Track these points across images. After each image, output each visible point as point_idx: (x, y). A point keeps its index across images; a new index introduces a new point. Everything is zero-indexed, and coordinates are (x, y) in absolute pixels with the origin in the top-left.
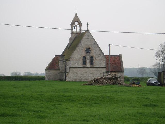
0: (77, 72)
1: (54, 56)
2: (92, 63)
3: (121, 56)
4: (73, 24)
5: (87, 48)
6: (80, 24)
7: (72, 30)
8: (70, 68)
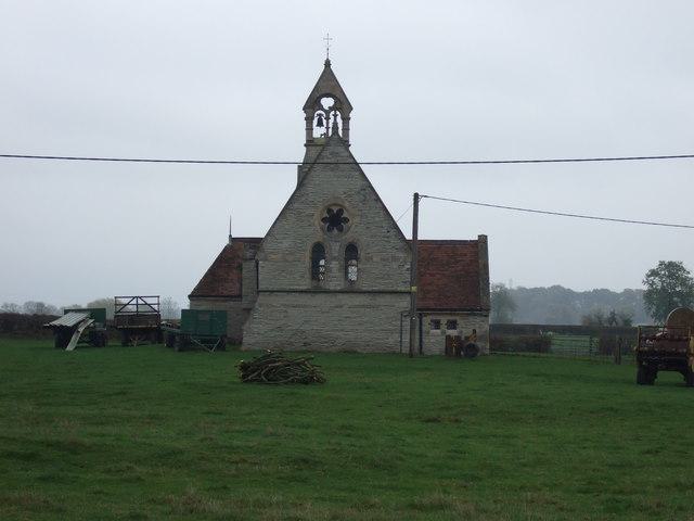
0: (286, 311)
1: (226, 242)
4: (312, 105)
5: (329, 211)
7: (309, 129)
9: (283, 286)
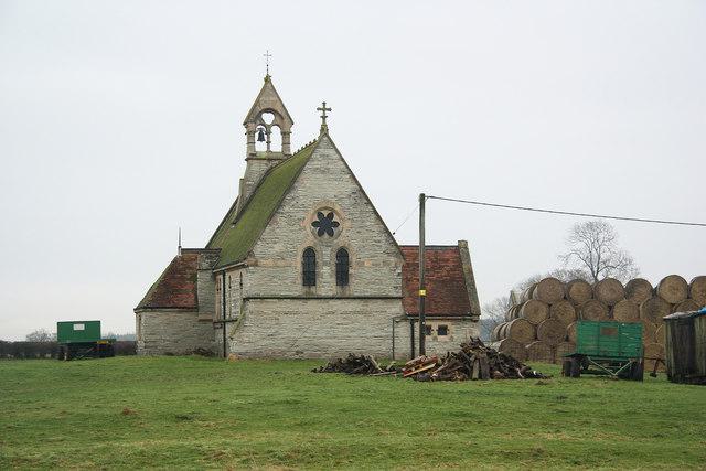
1: (175, 253)
2: (342, 276)
3: (466, 248)
4: (253, 118)
5: (320, 215)
6: (284, 120)
7: (251, 143)
8: (246, 300)
9: (273, 292)
